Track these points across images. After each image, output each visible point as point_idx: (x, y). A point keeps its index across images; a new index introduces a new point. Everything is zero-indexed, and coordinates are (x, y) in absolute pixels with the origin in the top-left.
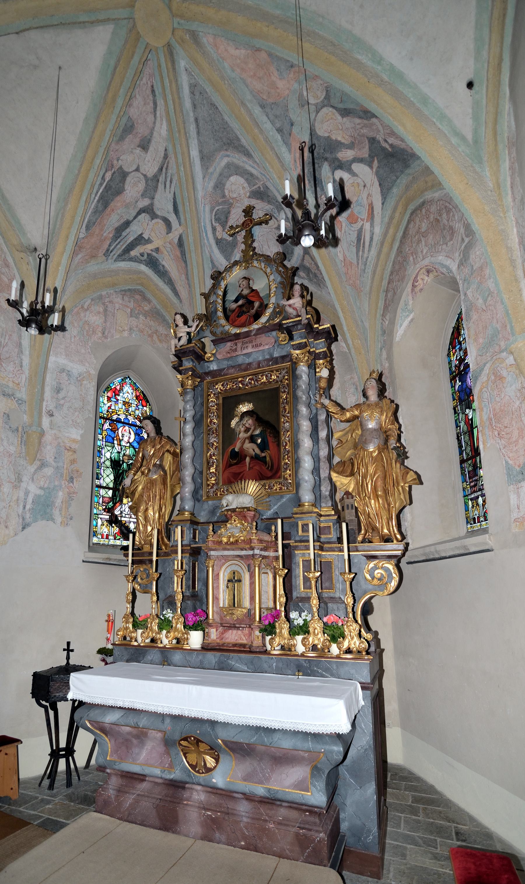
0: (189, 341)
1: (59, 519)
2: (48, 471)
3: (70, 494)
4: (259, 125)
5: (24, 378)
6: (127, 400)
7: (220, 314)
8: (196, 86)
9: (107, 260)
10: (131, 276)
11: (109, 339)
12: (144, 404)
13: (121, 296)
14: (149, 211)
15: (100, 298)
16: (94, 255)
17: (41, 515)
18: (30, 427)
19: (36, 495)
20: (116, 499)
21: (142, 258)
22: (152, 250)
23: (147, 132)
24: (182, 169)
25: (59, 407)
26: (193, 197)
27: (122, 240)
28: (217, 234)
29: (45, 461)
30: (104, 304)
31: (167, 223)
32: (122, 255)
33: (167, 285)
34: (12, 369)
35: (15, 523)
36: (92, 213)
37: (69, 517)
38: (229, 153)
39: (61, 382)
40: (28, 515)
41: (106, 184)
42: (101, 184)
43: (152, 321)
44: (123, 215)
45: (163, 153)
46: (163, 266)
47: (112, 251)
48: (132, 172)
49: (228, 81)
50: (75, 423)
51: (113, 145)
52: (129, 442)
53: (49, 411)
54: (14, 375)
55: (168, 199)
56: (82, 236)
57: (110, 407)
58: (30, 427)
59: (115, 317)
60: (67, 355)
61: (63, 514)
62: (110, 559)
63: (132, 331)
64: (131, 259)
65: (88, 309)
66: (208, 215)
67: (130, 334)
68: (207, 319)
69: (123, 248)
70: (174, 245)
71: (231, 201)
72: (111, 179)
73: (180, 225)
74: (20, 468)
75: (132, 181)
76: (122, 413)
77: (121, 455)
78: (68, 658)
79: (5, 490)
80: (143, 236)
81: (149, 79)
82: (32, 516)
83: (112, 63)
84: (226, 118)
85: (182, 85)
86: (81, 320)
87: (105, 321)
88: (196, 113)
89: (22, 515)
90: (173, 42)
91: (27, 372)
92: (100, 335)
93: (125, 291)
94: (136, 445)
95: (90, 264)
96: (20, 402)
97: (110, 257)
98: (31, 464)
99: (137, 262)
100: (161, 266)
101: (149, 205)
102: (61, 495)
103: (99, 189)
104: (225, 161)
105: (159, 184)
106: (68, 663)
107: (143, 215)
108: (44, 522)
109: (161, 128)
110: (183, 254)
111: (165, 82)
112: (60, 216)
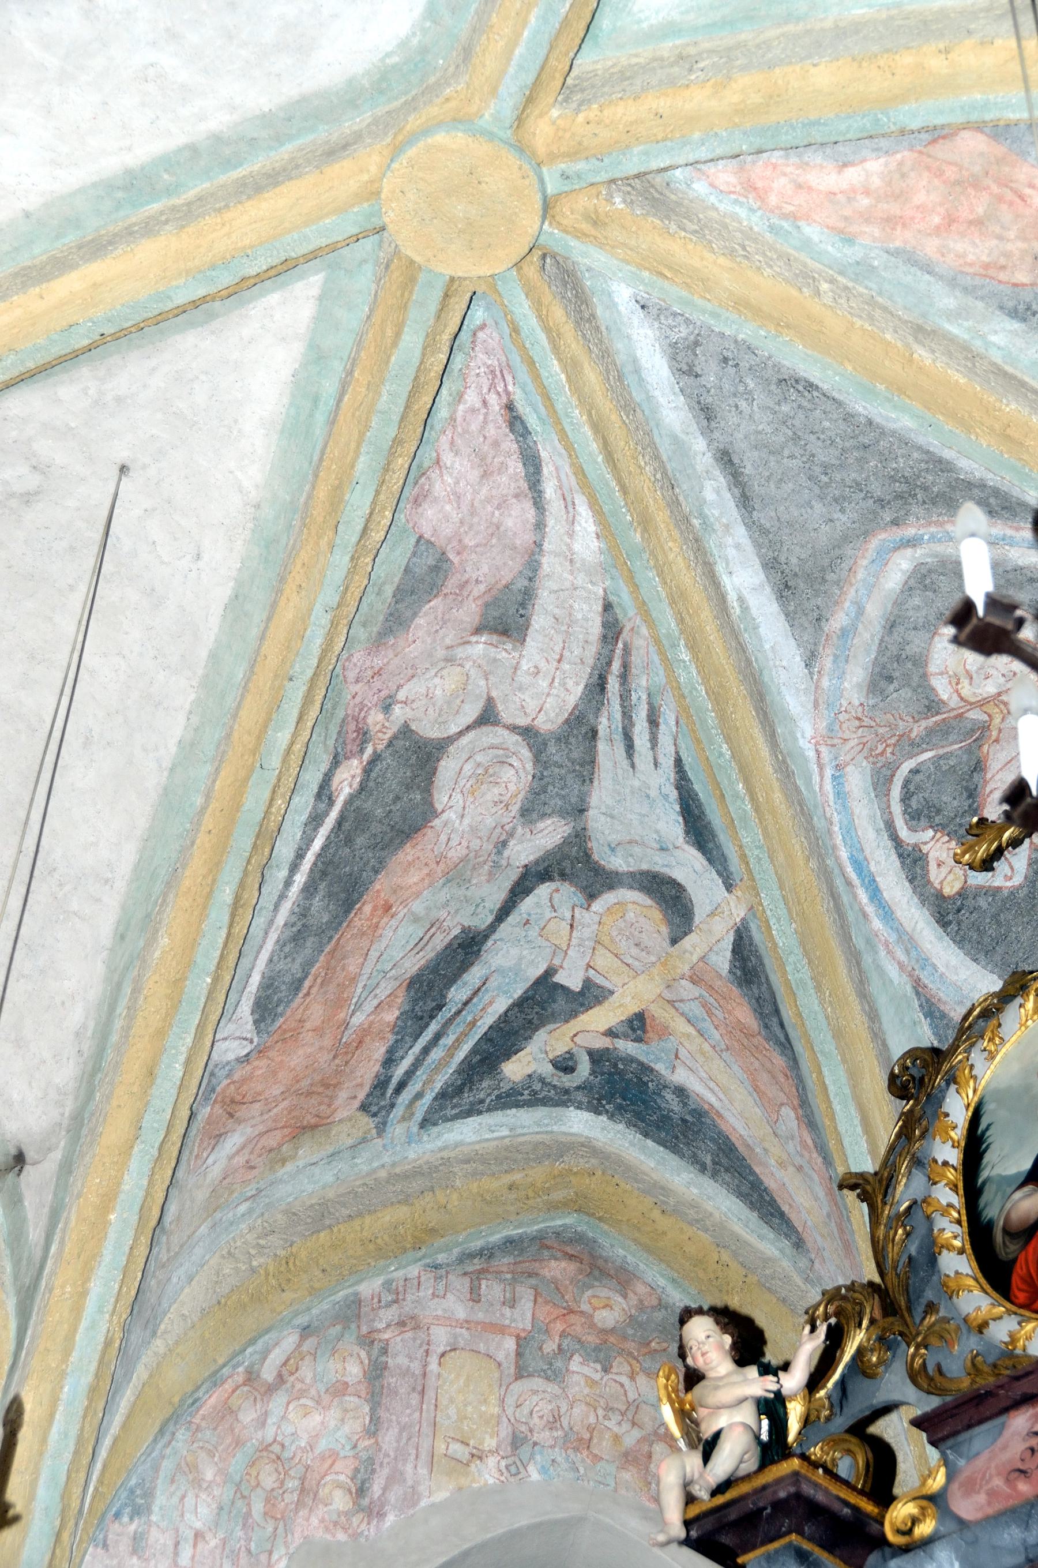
0: (773, 1449)
4: (1023, 384)
7: (957, 1263)
8: (697, 343)
9: (381, 1129)
11: (391, 1519)
13: (461, 1284)
14: (577, 867)
15: (352, 1312)
21: (567, 1081)
22: (610, 1033)
23: (509, 569)
24: (685, 656)
26: (765, 751)
27: (450, 1021)
28: (935, 875)
30: (367, 1341)
31: (670, 898)
32: (459, 1091)
33: (714, 1175)
36: (281, 944)
38: (911, 532)
42: (316, 820)
43: (642, 1379)
44: (443, 914)
45: (598, 621)
46: (681, 1092)
47: (401, 1086)
48: (461, 734)
49: (832, 281)
51: (358, 657)
55: (653, 793)
56: (229, 1050)
59: (430, 1394)
63: (525, 1451)
64: (511, 1098)
65: (280, 1379)
66: (864, 811)
67: (515, 1470)
68: (889, 1308)
70: (718, 983)
71: (976, 715)
72: (362, 788)
73: (729, 887)
75: (468, 768)
80: (559, 978)
81: (492, 386)
84: (861, 407)
85: (635, 361)
86: (238, 1443)
87: (374, 1428)
88: (716, 435)
90: (553, 236)
92: (341, 1501)
93: (487, 1253)
95: (289, 1167)
97: (398, 1112)
99: (545, 1102)
100: (669, 1096)
101: (566, 842)
103: (307, 841)
104: (903, 564)
105: (602, 746)
107: (544, 890)
109: (571, 534)
110: (769, 1011)
111: (544, 374)
112: (127, 990)
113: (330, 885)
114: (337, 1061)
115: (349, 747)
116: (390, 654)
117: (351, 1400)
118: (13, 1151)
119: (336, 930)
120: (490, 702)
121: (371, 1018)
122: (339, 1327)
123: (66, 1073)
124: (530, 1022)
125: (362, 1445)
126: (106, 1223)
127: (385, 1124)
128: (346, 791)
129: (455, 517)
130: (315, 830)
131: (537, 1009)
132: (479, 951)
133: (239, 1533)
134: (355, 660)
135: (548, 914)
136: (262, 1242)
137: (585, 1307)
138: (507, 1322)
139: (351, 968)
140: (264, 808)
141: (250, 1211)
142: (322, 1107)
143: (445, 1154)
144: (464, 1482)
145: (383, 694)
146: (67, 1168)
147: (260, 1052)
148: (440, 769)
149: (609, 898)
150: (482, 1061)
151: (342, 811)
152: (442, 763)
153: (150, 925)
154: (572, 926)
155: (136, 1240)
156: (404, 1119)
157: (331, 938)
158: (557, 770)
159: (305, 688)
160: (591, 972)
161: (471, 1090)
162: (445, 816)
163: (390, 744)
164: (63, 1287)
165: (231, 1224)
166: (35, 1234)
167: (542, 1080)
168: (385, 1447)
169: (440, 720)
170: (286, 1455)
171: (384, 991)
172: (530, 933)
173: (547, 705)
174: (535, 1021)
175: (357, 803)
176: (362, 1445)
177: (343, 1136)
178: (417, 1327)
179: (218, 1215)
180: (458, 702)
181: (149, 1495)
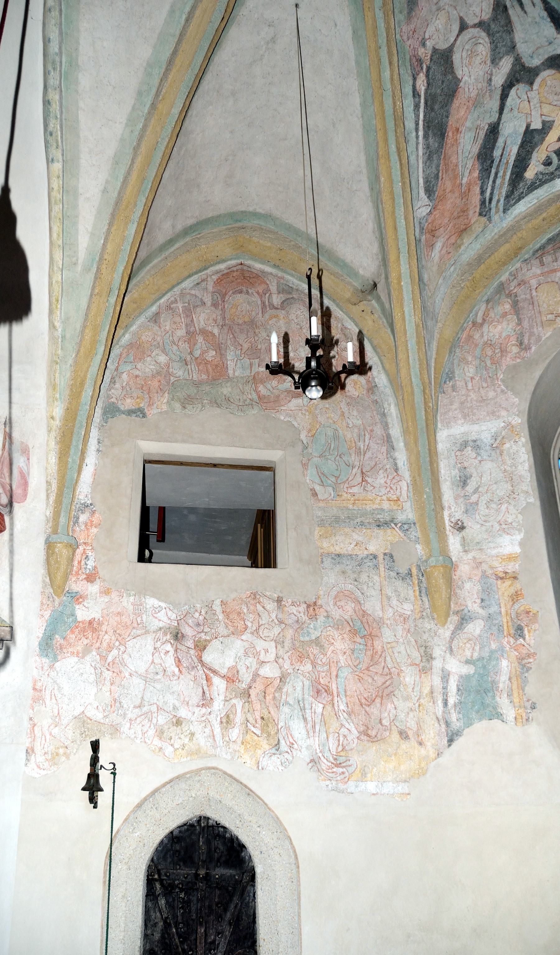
1: (510, 713)
2: (475, 628)
3: (523, 659)
5: (404, 487)
9: (490, 219)
10: (544, 215)
11: (533, 348)
13: (536, 262)
14: (522, 75)
16: (463, 227)
17: (478, 712)
19: (461, 677)
21: (551, 169)
25: (471, 508)
27: (498, 166)
30: (509, 295)
32: (512, 192)
34: (382, 481)
35: (433, 733)
36: (425, 163)
37: (528, 705)
39: (466, 464)
40: (454, 717)
44: (479, 122)
47: (491, 200)
48: (456, 40)
50: (504, 526)
51: (404, 28)
54: (388, 489)
55: (538, 19)
56: (423, 212)
59: (536, 303)
60: (465, 416)
61: (516, 700)
64: (533, 187)
65: (484, 320)
72: (428, 84)
74: (425, 637)
79: (407, 679)
80: (532, 127)
82: (461, 716)
86: (476, 345)
87: (520, 322)
89: (444, 718)
92: (515, 350)
93: (543, 247)
95: (463, 248)
96: (406, 527)
97: (493, 211)
98: (444, 625)
99: (546, 182)
101: (514, 65)
103: (417, 116)
105: (511, 12)
107: (513, 92)
108: (485, 723)
113: (433, 130)
114: (463, 200)
115: (417, 70)
116: (416, 20)
117: (509, 317)
118: (372, 283)
119: (442, 148)
120: (461, 19)
121: (469, 178)
122: (498, 295)
123: (375, 248)
124: (528, 151)
125: (517, 329)
126: (401, 286)
127: (490, 217)
128: (423, 88)
130: (418, 110)
131: (529, 144)
132: (498, 131)
133: (485, 372)
134: (404, 30)
135: (518, 101)
136: (463, 278)
138: (556, 267)
139: (454, 161)
140: (392, 107)
141: (455, 269)
142: (466, 220)
143: (516, 219)
144: (555, 326)
145: (420, 39)
146: (387, 278)
147: (434, 208)
148: (454, 61)
149: (538, 80)
150: (516, 176)
151: (425, 98)
152: (454, 57)
153: (377, 178)
154: (529, 101)
155: (413, 288)
156: (496, 212)
157: (442, 152)
158: (498, 35)
159: (386, 48)
160: (543, 117)
161: (517, 190)
162: (464, 80)
163: (431, 60)
164: (397, 315)
165: (450, 276)
166: (387, 306)
167: (541, 173)
168: (525, 326)
169: (446, 38)
170: (493, 343)
171: (469, 166)
172: (514, 113)
173: (484, 7)
174: (530, 150)
175: (429, 91)
176: (517, 329)
177: (477, 228)
178: (525, 283)
179: (444, 274)
180: (449, 26)
181: (453, 373)
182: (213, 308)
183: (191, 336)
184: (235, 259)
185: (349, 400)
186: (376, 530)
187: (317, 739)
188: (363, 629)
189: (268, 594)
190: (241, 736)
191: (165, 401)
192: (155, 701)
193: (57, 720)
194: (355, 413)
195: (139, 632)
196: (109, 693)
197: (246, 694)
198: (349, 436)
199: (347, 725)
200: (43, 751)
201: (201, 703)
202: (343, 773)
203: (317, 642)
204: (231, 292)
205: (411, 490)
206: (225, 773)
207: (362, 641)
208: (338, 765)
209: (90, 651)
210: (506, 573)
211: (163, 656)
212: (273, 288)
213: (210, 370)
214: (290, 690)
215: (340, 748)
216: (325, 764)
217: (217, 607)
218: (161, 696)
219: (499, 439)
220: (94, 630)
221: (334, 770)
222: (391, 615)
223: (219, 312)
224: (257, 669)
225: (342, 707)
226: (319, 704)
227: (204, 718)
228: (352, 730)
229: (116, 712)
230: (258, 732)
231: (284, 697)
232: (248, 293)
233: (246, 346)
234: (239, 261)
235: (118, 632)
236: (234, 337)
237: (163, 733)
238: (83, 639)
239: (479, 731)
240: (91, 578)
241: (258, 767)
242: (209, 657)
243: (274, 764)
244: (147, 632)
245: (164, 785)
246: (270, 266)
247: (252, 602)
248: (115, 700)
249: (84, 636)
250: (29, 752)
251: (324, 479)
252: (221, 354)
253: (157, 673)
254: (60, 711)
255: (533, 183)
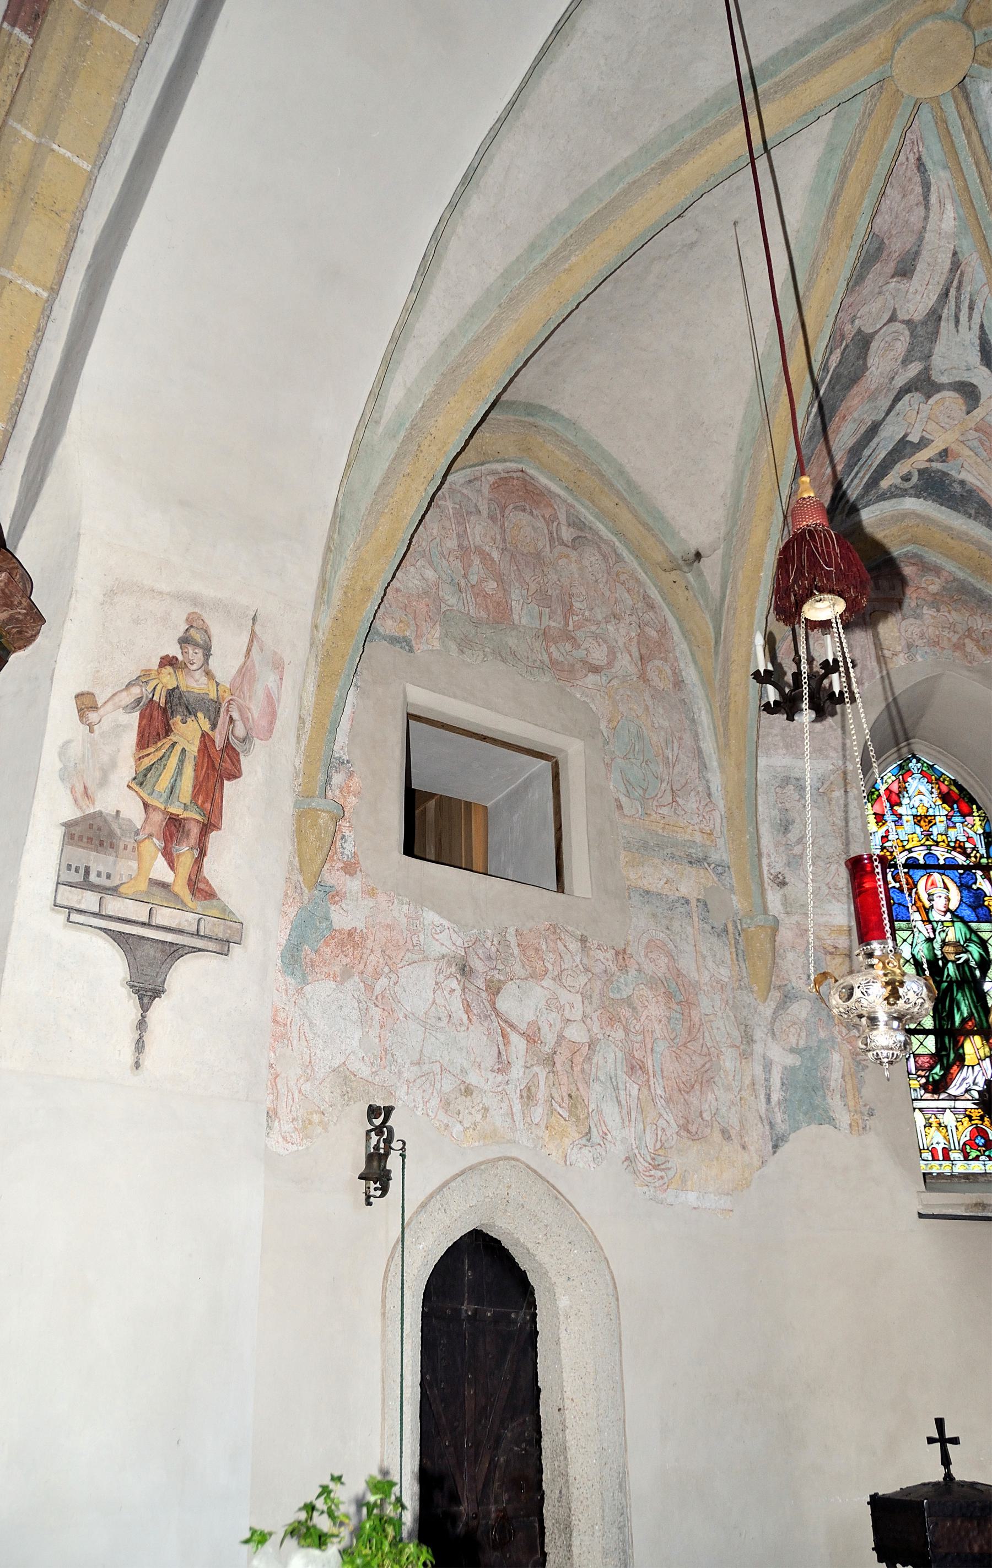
1: (844, 1119)
2: (800, 1010)
3: (858, 1054)
6: (921, 811)
11: (866, 684)
12: (965, 809)
14: (925, 385)
17: (806, 1114)
18: (752, 919)
19: (785, 1068)
20: (948, 1056)
21: (907, 485)
22: (930, 460)
29: (789, 987)
34: (694, 806)
35: (757, 1136)
39: (788, 806)
40: (778, 1117)
41: (831, 377)
43: (953, 613)
46: (962, 483)
50: (834, 891)
52: (948, 910)
53: (777, 877)
54: (701, 818)
55: (967, 343)
57: (885, 838)
58: (752, 919)
60: (787, 746)
61: (851, 1103)
62: (984, 1206)
63: (913, 650)
64: (883, 497)
69: (865, 480)
76: (915, 843)
77: (937, 945)
78: (946, 1461)
82: (786, 1117)
83: (836, 164)
89: (768, 1118)
91: (721, 804)
94: (967, 913)
99: (895, 497)
101: (920, 373)
102: (837, 1061)
105: (943, 324)
106: (948, 1476)
107: (907, 397)
108: (814, 1128)
112: (747, 474)
120: (895, 310)
123: (719, 514)
128: (834, 365)
129: (889, 220)
137: (924, 585)
149: (937, 397)
167: (896, 486)
182: (489, 521)
183: (464, 551)
184: (516, 462)
185: (653, 692)
186: (688, 868)
187: (633, 1129)
188: (678, 993)
189: (569, 928)
190: (545, 1117)
191: (437, 635)
192: (438, 1058)
193: (309, 1071)
194: (661, 710)
195: (415, 957)
196: (377, 1040)
197: (550, 1061)
198: (655, 739)
199: (665, 1115)
200: (291, 1117)
201: (496, 1067)
202: (662, 1178)
203: (628, 1001)
204: (511, 506)
205: (725, 824)
206: (528, 1166)
207: (678, 1008)
208: (656, 1167)
209: (351, 976)
210: (836, 948)
211: (448, 996)
212: (562, 518)
213: (490, 607)
214: (601, 1062)
215: (659, 1145)
216: (641, 1165)
217: (513, 940)
218: (446, 1052)
219: (827, 784)
220: (355, 946)
221: (652, 1173)
222: (708, 979)
223: (498, 531)
224: (562, 1029)
225: (660, 1092)
226: (635, 1085)
227: (500, 1089)
228: (670, 1121)
229: (388, 1068)
230: (565, 1115)
231: (594, 1070)
232: (531, 513)
233: (533, 587)
234: (520, 466)
235: (387, 952)
236: (518, 570)
237: (449, 1104)
238: (341, 956)
239: (806, 1140)
240: (350, 868)
241: (565, 1162)
242: (505, 1003)
243: (585, 1159)
244: (426, 959)
245: (454, 1178)
246: (560, 486)
247: (552, 937)
248: (386, 1051)
249: (343, 952)
250: (272, 1115)
251: (630, 788)
252: (504, 590)
253: (440, 1019)
254: (313, 1058)
255: (884, 493)
